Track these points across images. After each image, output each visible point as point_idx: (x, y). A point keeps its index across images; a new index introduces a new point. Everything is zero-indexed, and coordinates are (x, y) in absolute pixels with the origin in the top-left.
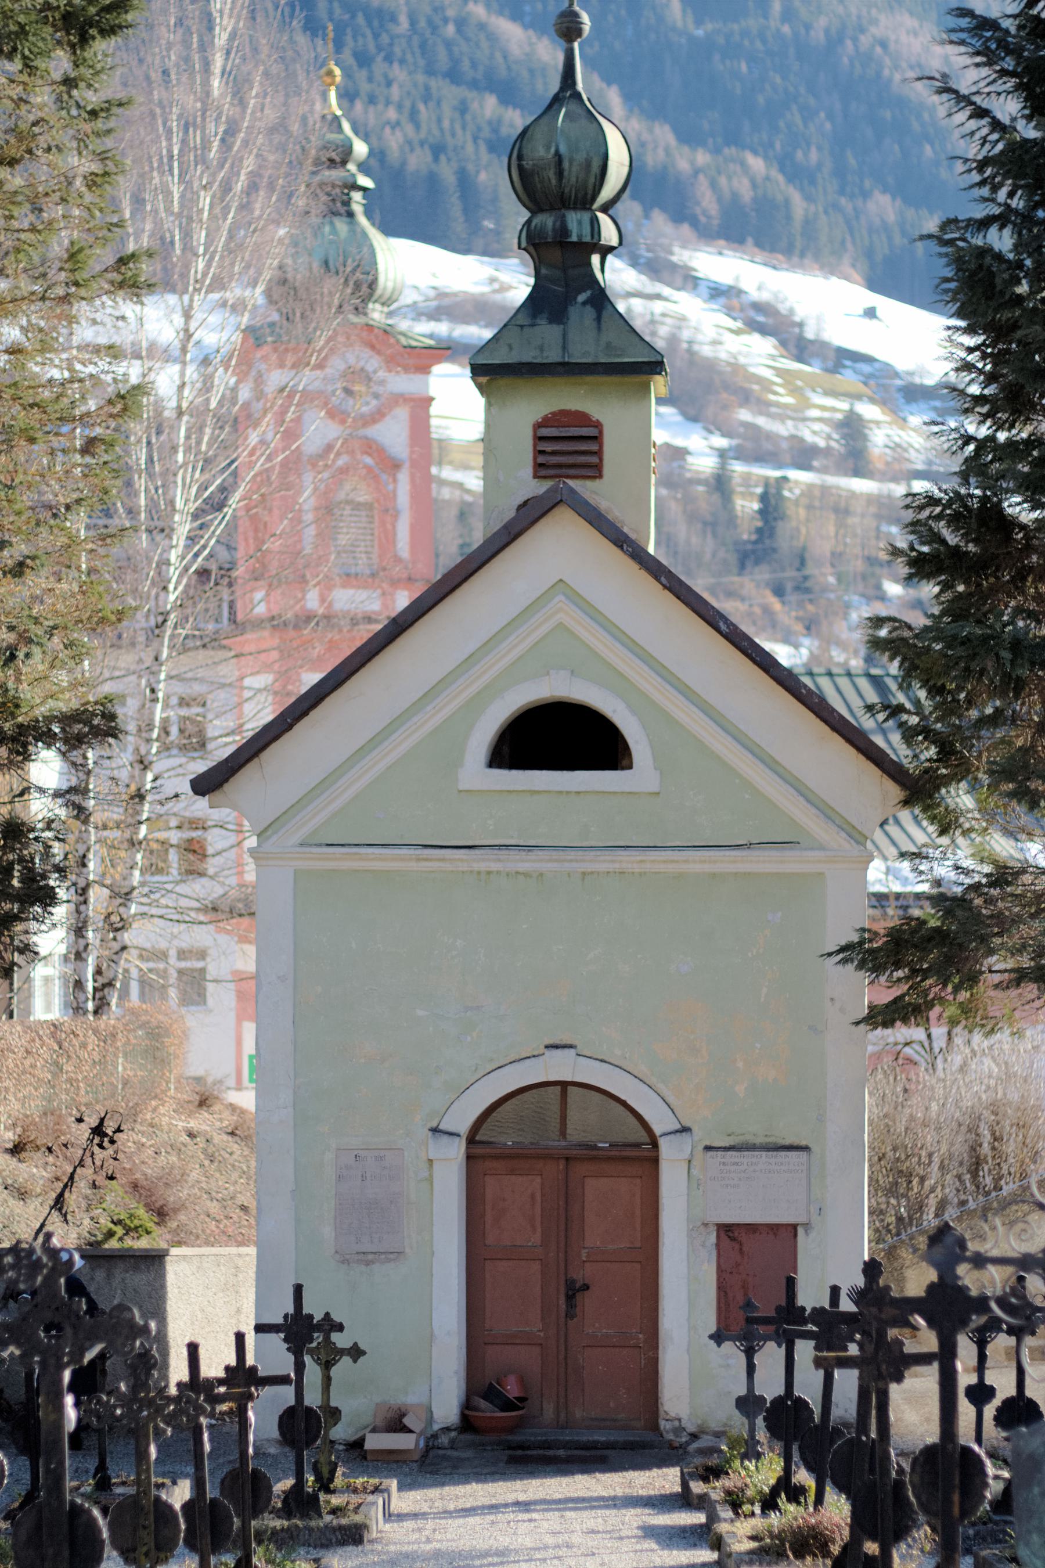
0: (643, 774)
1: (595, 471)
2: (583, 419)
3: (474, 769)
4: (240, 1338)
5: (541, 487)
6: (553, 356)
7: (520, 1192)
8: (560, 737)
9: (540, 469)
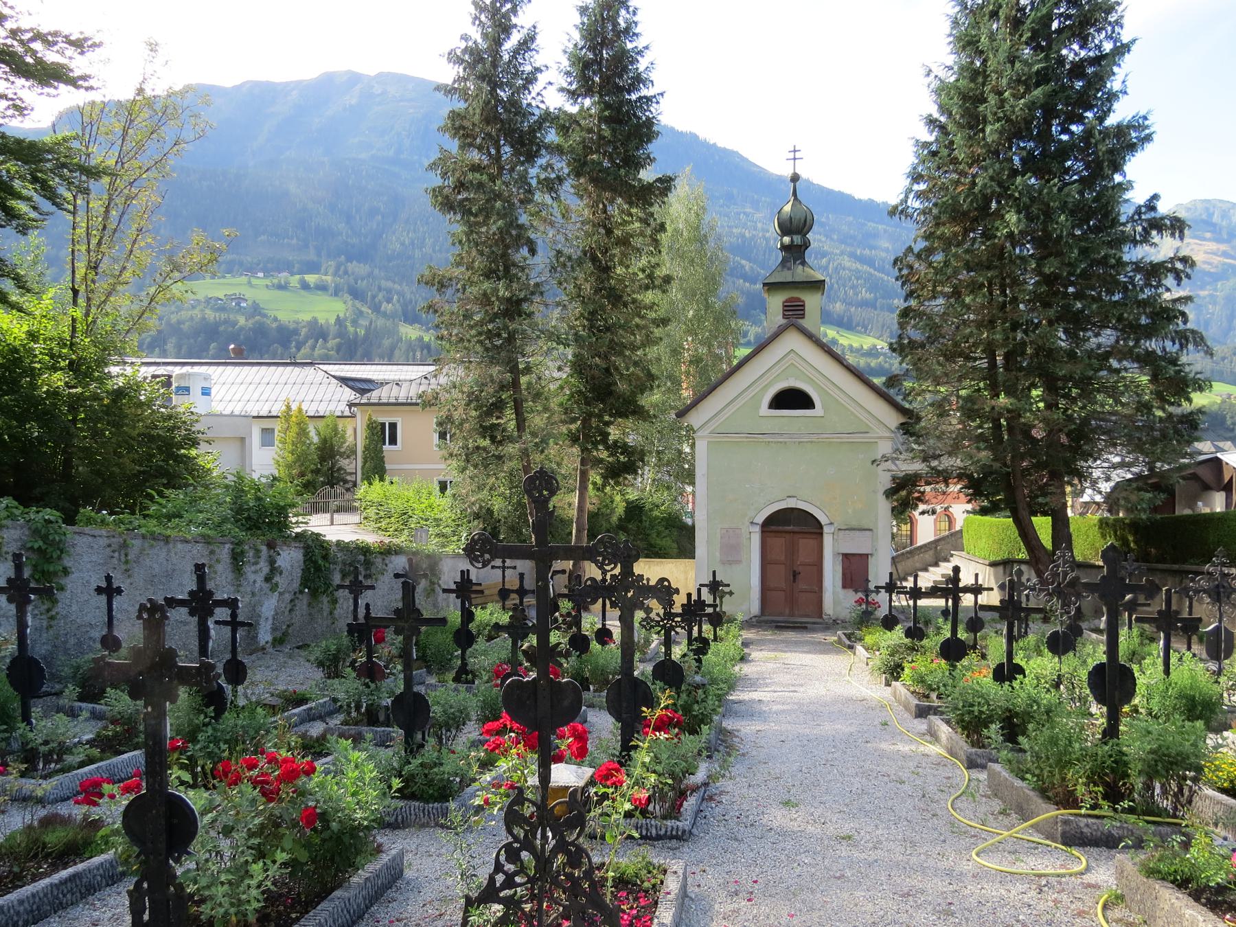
0: (819, 410)
1: (803, 316)
2: (799, 300)
3: (764, 410)
4: (728, 585)
5: (784, 321)
6: (790, 280)
7: (778, 543)
8: (792, 399)
9: (785, 316)
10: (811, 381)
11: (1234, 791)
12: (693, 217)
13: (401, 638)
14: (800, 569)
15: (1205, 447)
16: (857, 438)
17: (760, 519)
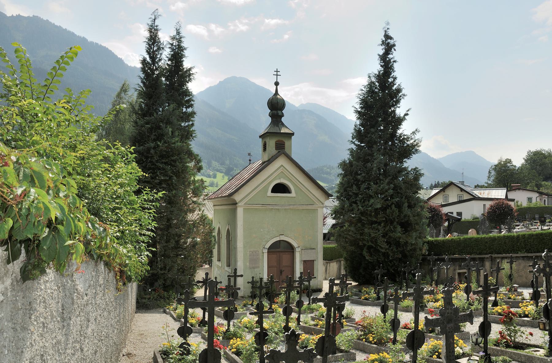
0: (293, 194)
3: (269, 193)
8: (280, 188)
9: (276, 149)
10: (290, 181)
11: (15, 362)
12: (175, 43)
13: (206, 328)
14: (283, 269)
15: (359, 110)
16: (310, 207)
17: (268, 246)
